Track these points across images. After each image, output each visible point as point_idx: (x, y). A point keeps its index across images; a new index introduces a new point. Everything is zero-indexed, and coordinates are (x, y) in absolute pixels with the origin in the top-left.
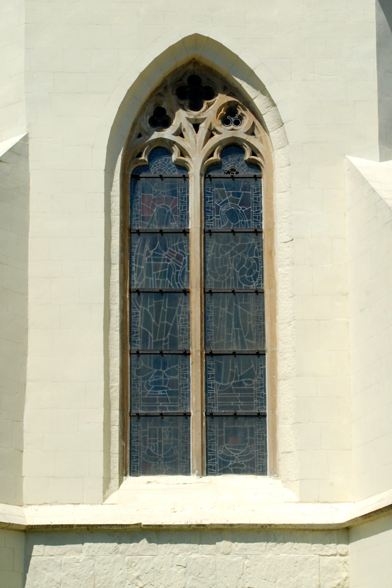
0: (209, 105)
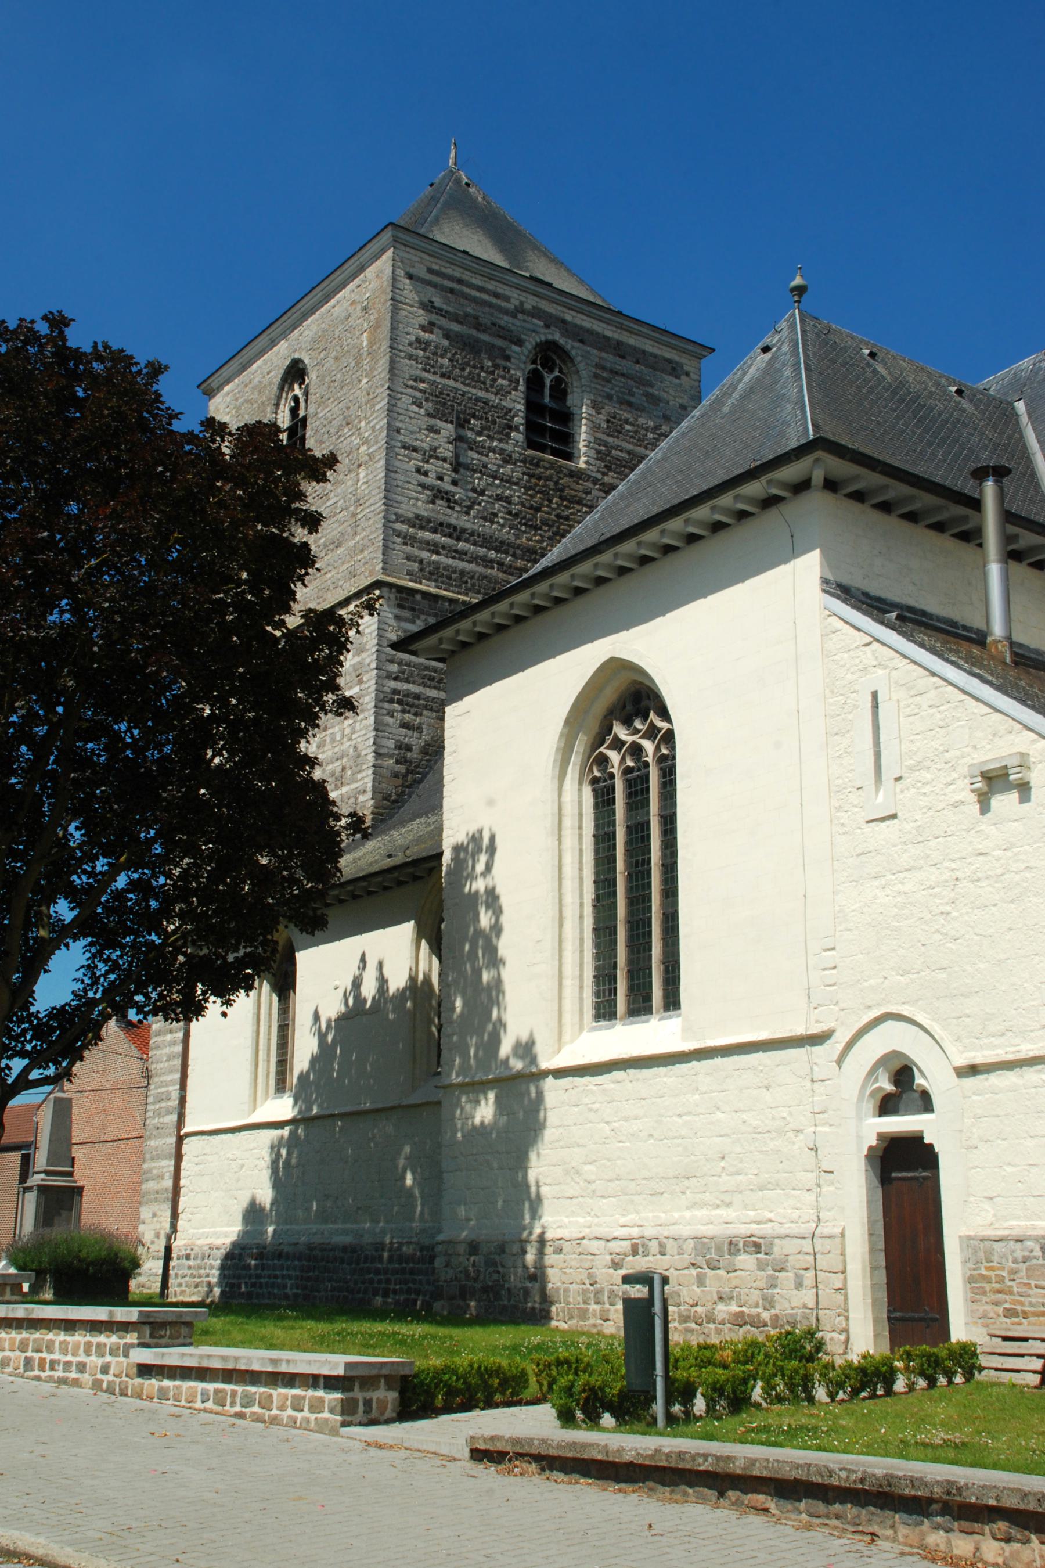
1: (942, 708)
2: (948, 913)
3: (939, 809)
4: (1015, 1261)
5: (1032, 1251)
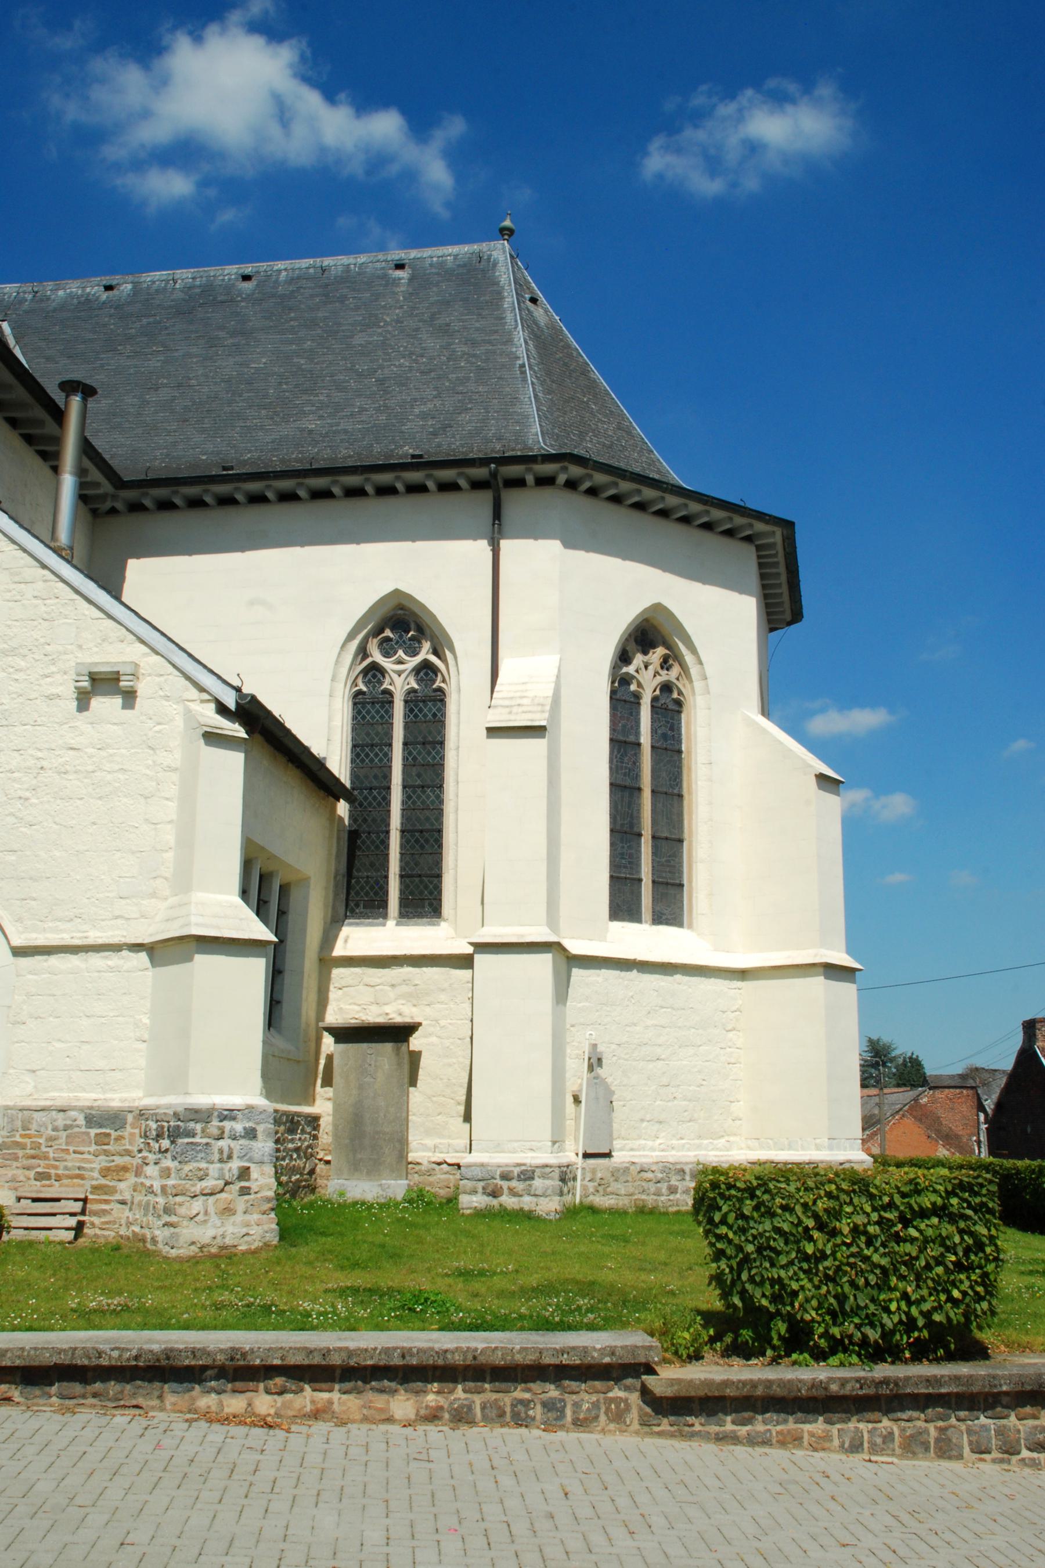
0: (654, 653)
1: (48, 602)
2: (27, 799)
3: (31, 697)
4: (55, 1129)
5: (75, 1120)
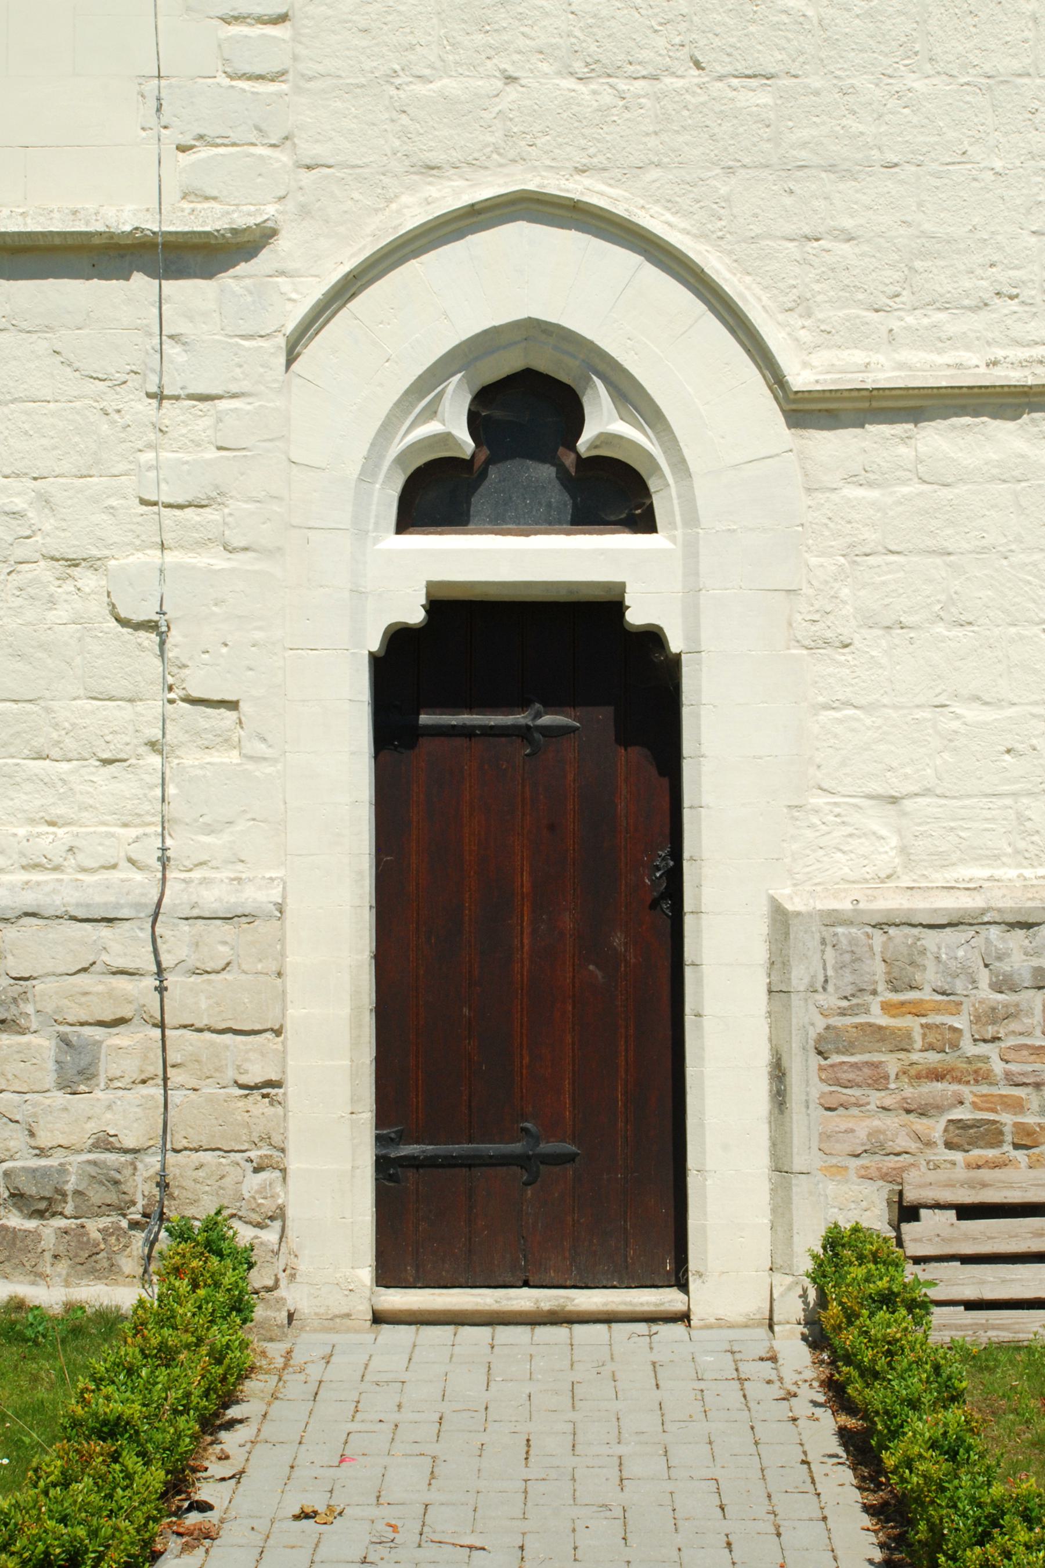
4: (1003, 984)
